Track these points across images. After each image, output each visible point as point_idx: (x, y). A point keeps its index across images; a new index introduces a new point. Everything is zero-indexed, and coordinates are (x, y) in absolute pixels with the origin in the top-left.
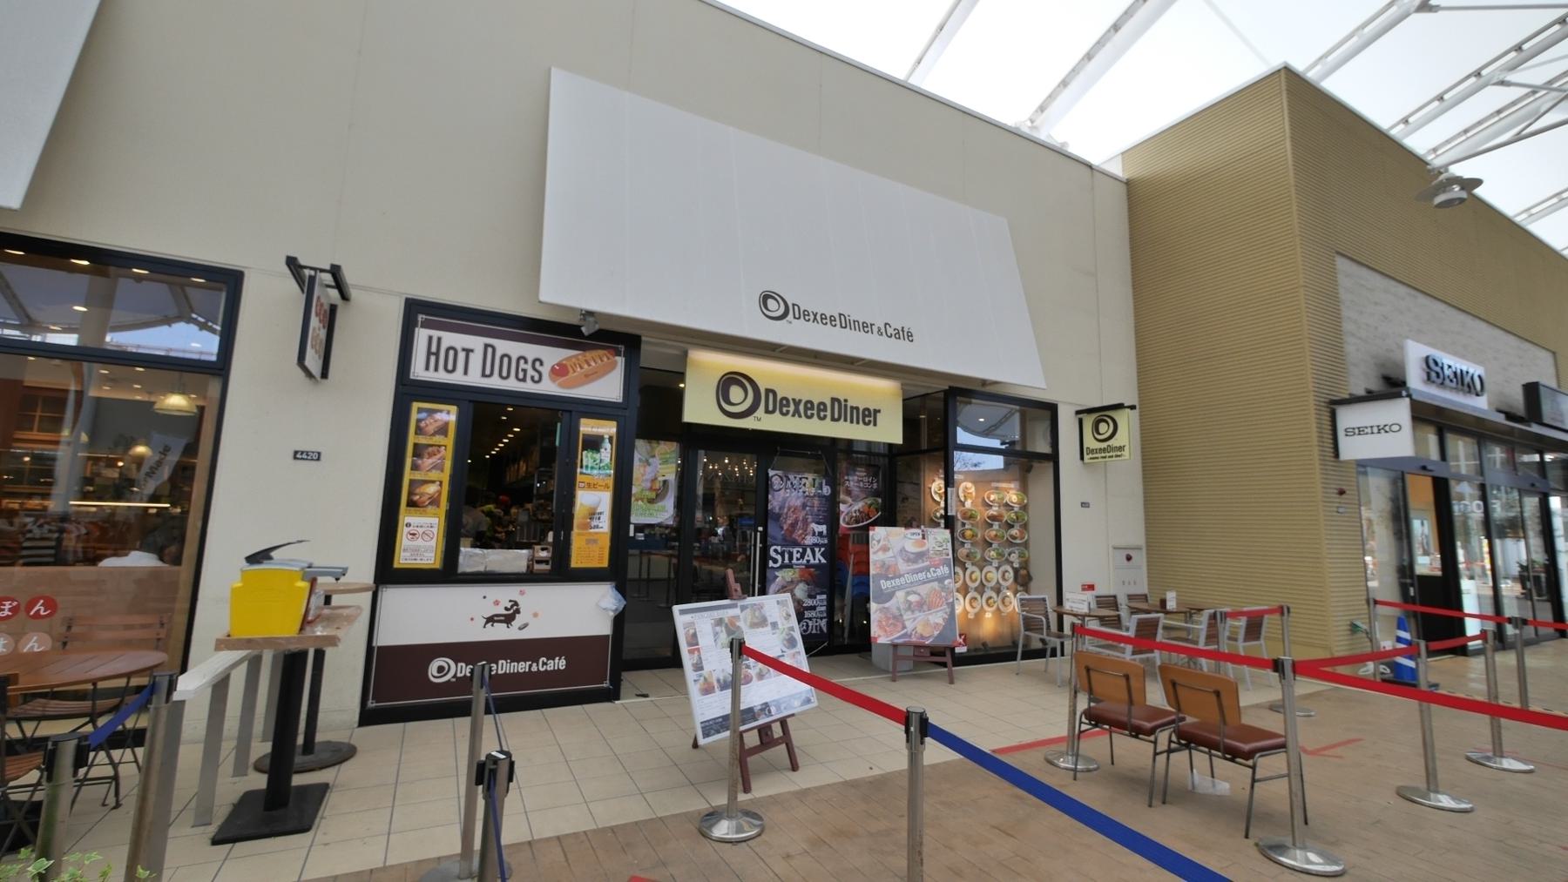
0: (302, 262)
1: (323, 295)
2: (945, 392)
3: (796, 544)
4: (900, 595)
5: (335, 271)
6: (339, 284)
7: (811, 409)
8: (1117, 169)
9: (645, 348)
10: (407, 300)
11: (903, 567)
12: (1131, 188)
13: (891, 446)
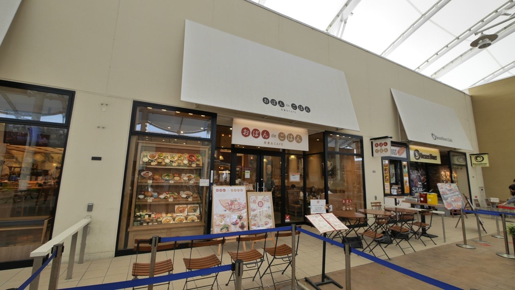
2: (324, 133)
3: (417, 187)
4: (449, 198)
7: (426, 157)
8: (467, 92)
9: (218, 119)
10: (134, 101)
11: (448, 192)
12: (473, 99)
13: (304, 152)
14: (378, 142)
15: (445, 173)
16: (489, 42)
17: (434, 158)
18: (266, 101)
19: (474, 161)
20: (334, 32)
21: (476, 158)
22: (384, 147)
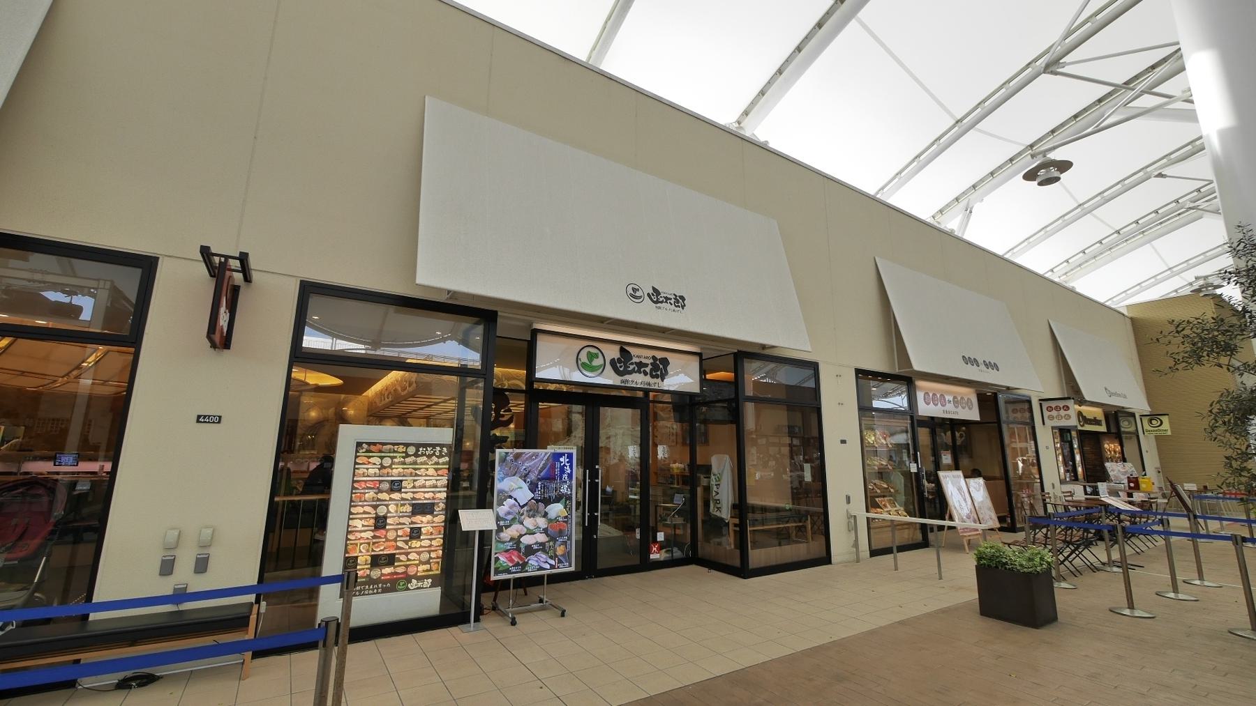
0: (213, 250)
1: (227, 280)
5: (243, 258)
6: (245, 270)
14: (1053, 404)
15: (1110, 447)
16: (1056, 174)
17: (1097, 422)
18: (967, 360)
19: (1147, 427)
20: (951, 223)
21: (1150, 421)
22: (1062, 412)
